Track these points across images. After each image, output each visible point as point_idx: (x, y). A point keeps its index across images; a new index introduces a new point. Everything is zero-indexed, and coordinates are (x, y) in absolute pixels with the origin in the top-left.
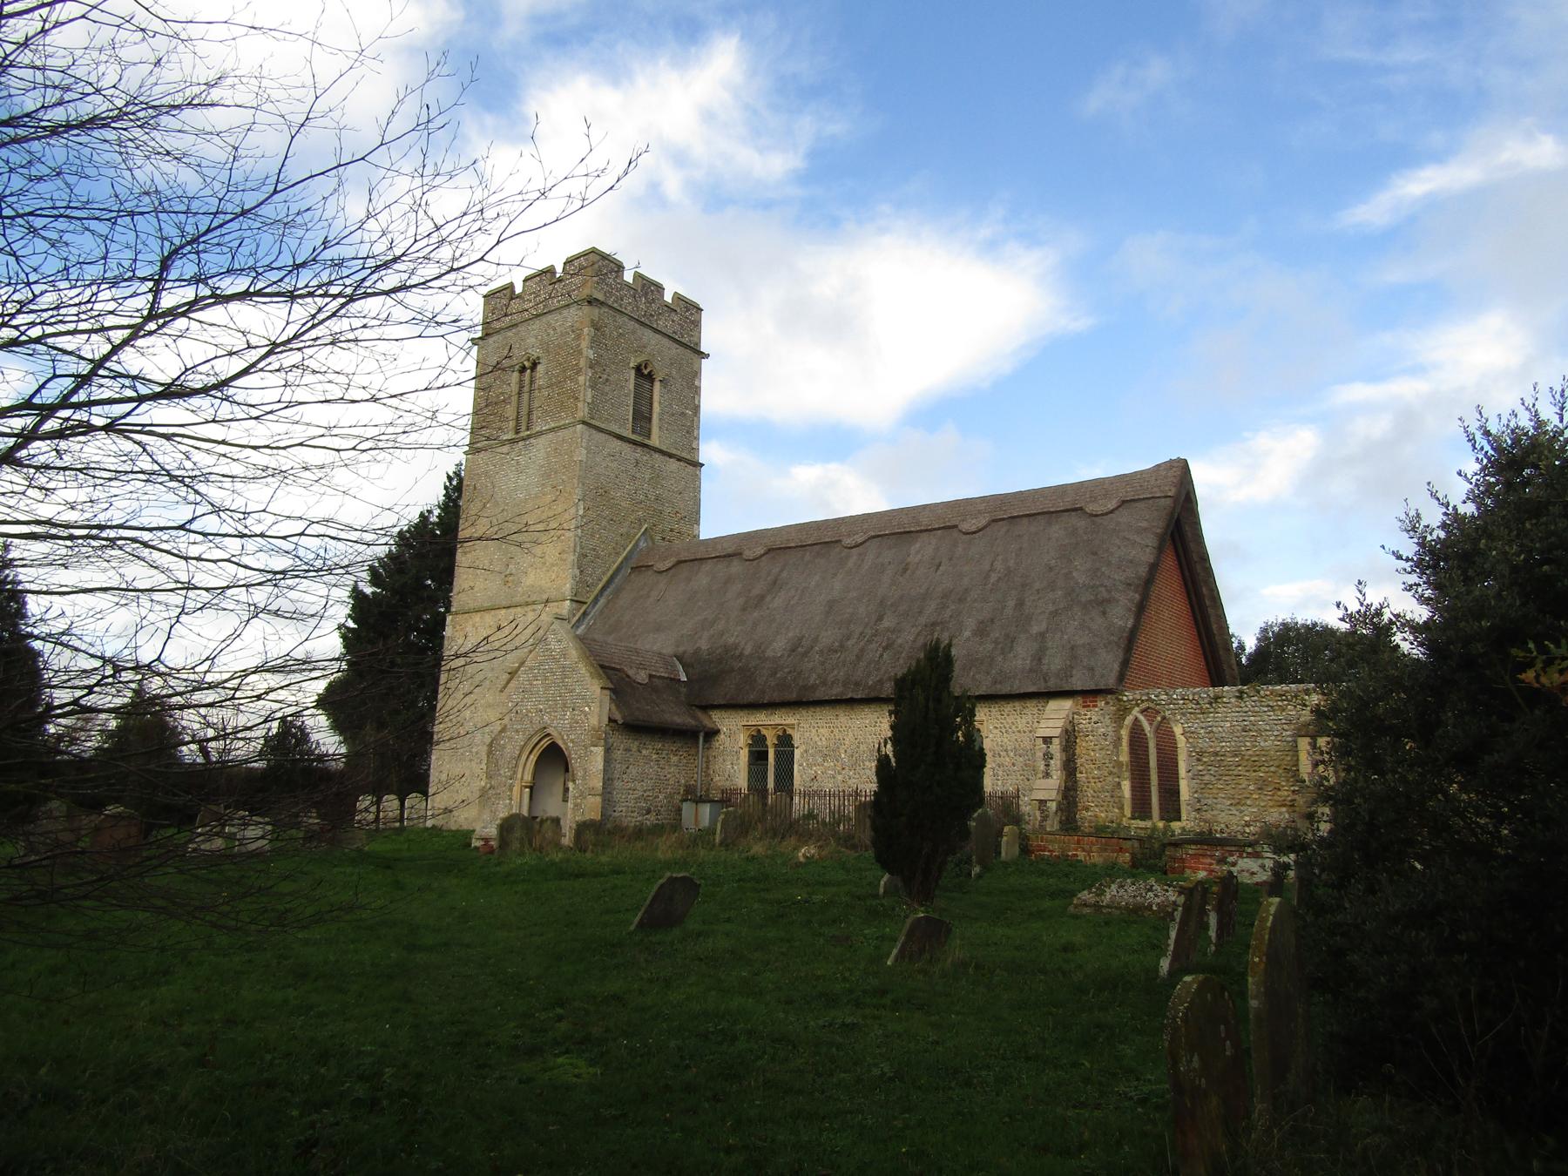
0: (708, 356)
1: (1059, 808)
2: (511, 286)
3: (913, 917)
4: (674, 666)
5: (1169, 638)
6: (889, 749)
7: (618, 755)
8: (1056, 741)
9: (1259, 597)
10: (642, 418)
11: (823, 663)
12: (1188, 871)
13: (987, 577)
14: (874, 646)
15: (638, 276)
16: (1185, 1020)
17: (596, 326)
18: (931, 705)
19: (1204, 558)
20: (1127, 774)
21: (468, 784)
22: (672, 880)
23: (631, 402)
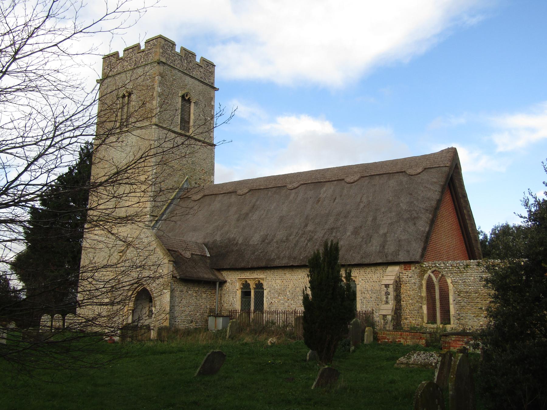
0: (218, 89)
1: (393, 319)
2: (117, 54)
3: (322, 368)
4: (203, 249)
5: (447, 235)
6: (309, 292)
7: (177, 293)
8: (391, 286)
9: (488, 217)
10: (185, 122)
11: (278, 248)
12: (452, 348)
13: (359, 205)
14: (303, 239)
15: (183, 49)
16: (421, 396)
17: (161, 75)
18: (330, 271)
19: (465, 196)
20: (425, 302)
21: (95, 310)
22: (213, 353)
23: (179, 117)
